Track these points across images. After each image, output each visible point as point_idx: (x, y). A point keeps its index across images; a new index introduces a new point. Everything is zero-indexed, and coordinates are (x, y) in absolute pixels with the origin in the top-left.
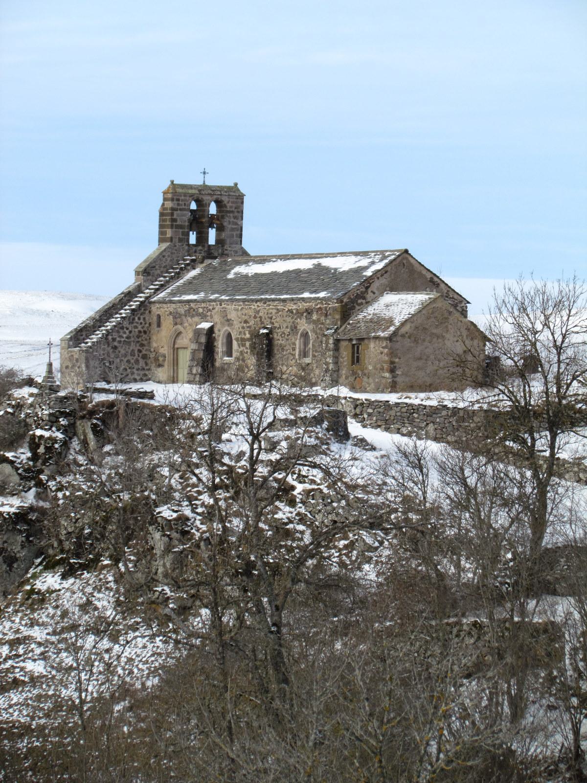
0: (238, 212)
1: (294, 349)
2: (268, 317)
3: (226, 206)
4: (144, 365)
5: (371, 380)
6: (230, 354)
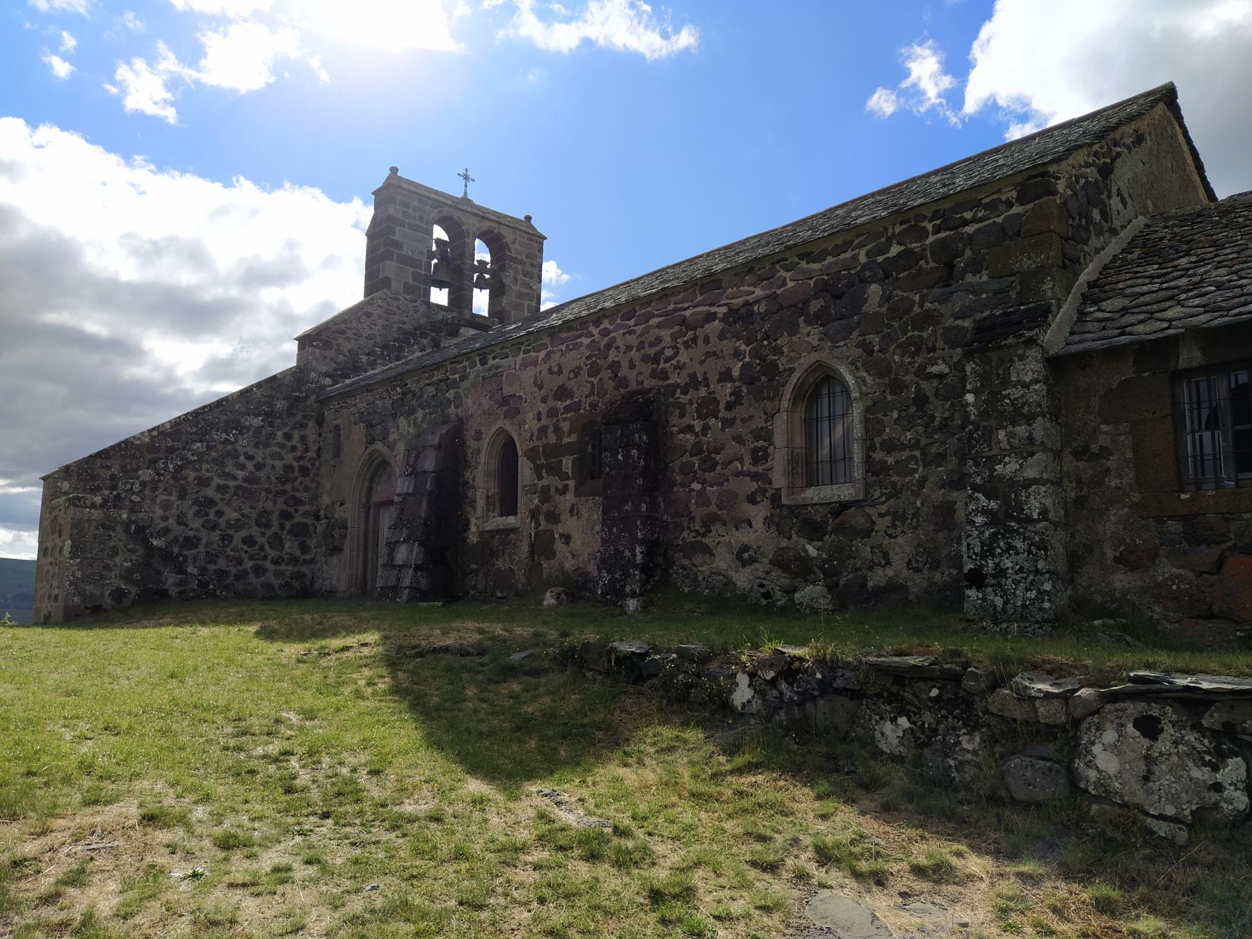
0: (533, 265)
1: (760, 456)
2: (645, 359)
3: (509, 249)
4: (297, 553)
6: (509, 508)
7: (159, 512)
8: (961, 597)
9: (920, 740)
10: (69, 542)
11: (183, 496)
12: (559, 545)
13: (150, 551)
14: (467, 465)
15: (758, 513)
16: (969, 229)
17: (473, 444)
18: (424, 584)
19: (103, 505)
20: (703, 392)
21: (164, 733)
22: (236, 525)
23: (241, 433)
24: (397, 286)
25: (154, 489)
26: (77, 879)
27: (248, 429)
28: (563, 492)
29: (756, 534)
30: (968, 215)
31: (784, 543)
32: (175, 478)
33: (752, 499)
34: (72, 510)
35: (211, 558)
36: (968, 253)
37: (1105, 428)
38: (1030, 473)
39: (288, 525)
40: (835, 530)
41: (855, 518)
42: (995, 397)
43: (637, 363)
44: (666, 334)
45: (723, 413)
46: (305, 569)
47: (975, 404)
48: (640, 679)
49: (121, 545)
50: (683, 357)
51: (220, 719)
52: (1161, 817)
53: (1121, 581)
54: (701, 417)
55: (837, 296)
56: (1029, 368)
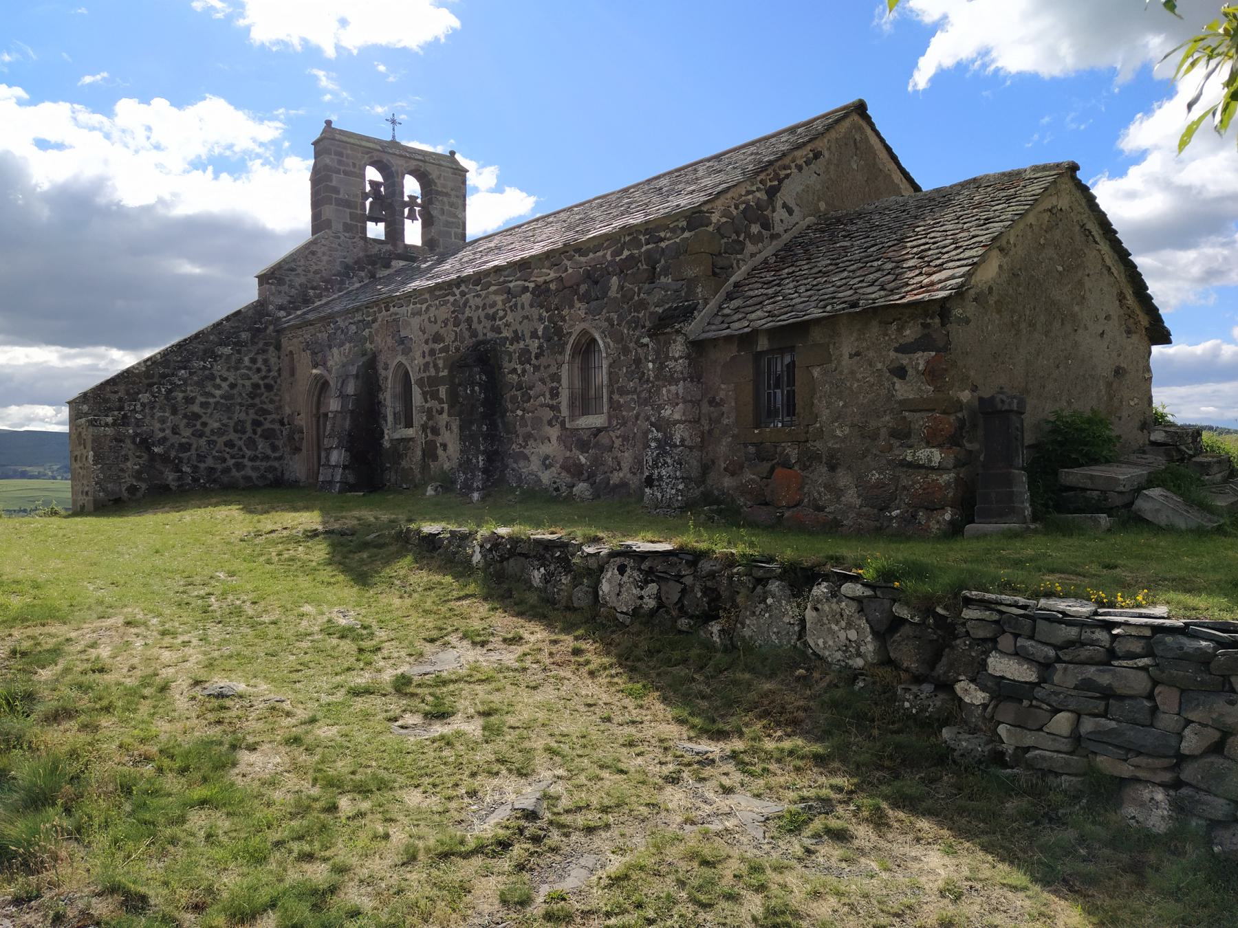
1: (555, 394)
2: (487, 317)
3: (435, 184)
4: (269, 452)
5: (844, 479)
7: (158, 425)
8: (643, 493)
9: (547, 579)
10: (91, 453)
11: (174, 411)
12: (440, 452)
13: (153, 457)
14: (380, 389)
15: (554, 433)
16: (663, 245)
17: (383, 373)
18: (351, 479)
19: (114, 424)
20: (522, 345)
21: (144, 585)
22: (220, 432)
23: (215, 361)
24: (337, 226)
25: (152, 408)
26: (94, 645)
27: (221, 356)
28: (441, 412)
29: (552, 448)
30: (662, 234)
31: (568, 454)
32: (167, 398)
33: (550, 424)
34: (91, 429)
35: (201, 458)
36: (663, 261)
37: (723, 386)
38: (677, 417)
39: (259, 430)
40: (594, 446)
41: (604, 439)
42: (662, 367)
43: (482, 319)
44: (499, 299)
45: (534, 361)
46: (276, 464)
47: (653, 370)
48: (435, 549)
49: (130, 453)
50: (510, 318)
51: (177, 577)
52: (622, 613)
53: (728, 482)
54: (522, 363)
55: (596, 283)
56: (678, 348)
